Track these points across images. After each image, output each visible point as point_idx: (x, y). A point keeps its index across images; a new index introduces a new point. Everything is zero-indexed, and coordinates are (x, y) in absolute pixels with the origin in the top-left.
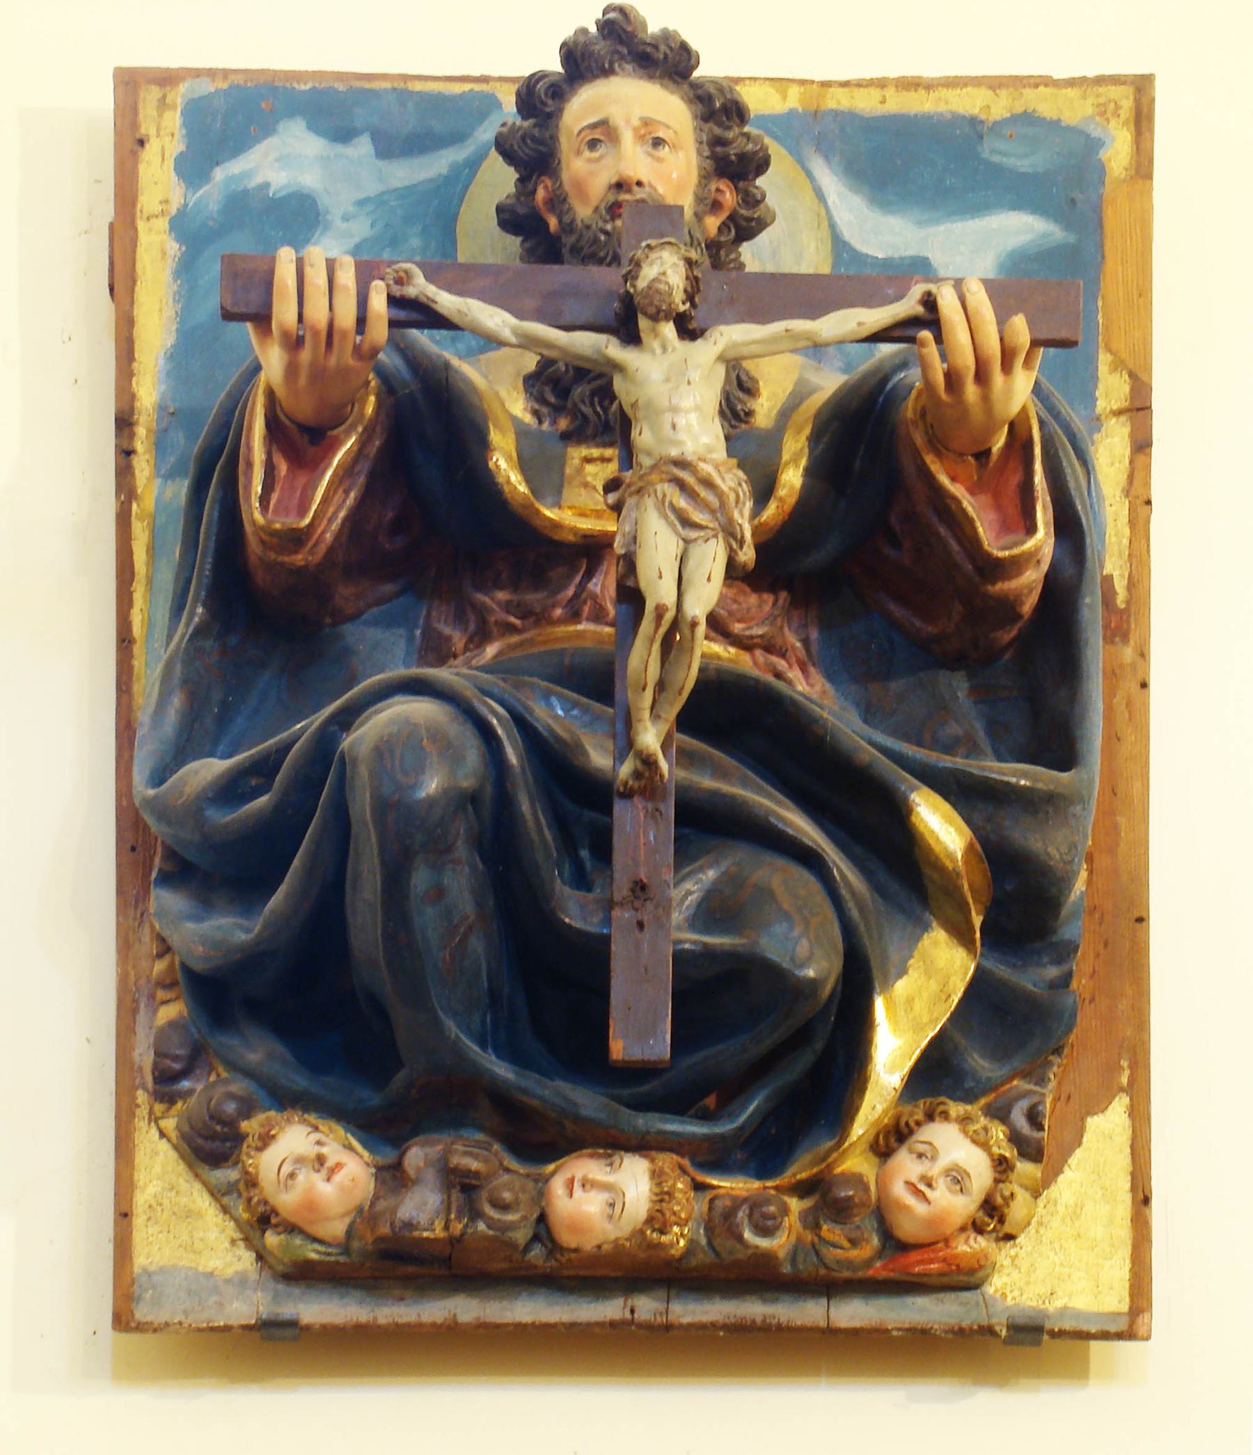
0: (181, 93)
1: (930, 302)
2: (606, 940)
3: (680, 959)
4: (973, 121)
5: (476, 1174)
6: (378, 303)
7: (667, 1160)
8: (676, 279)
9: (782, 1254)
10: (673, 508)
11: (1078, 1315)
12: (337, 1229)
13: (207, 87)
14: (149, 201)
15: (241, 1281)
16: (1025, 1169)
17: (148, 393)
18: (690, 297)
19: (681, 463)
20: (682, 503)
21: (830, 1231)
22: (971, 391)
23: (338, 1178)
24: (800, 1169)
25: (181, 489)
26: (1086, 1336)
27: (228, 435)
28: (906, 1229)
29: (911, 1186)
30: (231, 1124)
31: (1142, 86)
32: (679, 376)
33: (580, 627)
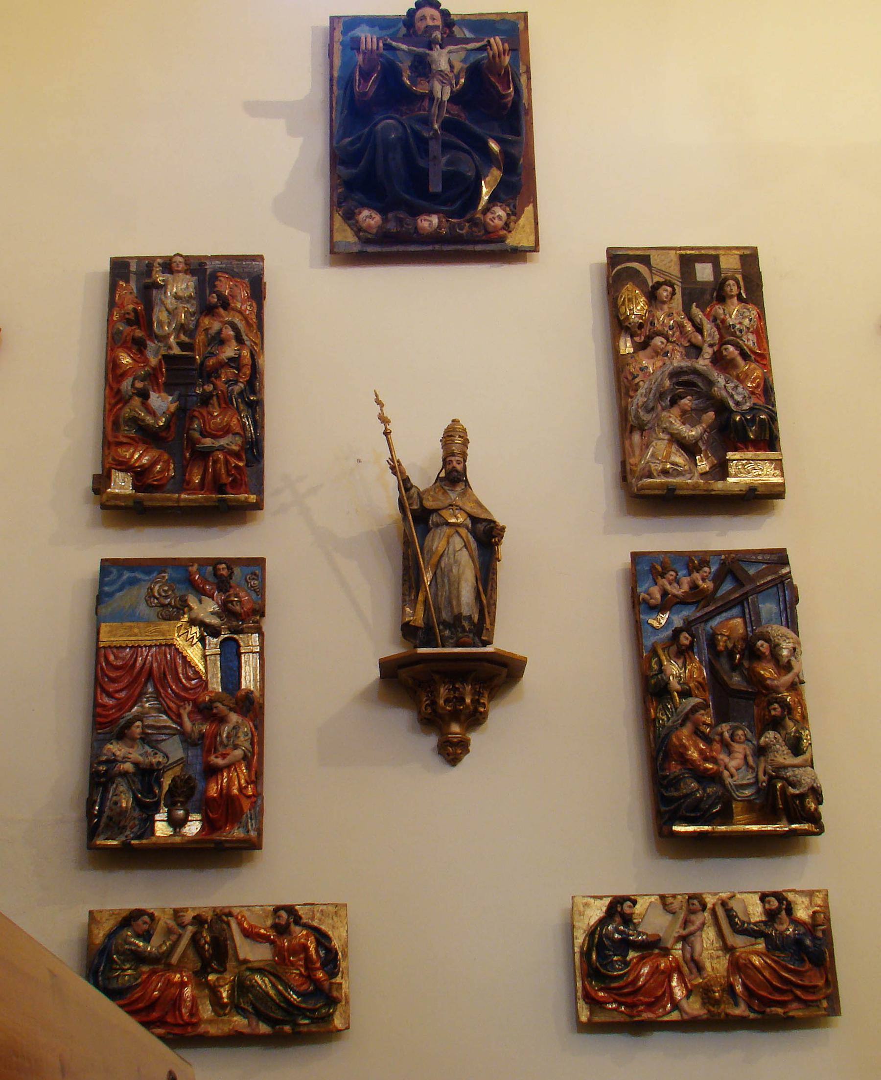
0: (342, 20)
1: (489, 42)
2: (428, 169)
3: (443, 172)
4: (493, 20)
5: (402, 218)
6: (381, 44)
7: (441, 215)
8: (439, 36)
9: (465, 234)
10: (440, 80)
11: (526, 247)
12: (374, 231)
13: (347, 19)
14: (336, 39)
15: (355, 243)
16: (513, 217)
17: (336, 74)
18: (442, 40)
19: (441, 71)
20: (441, 79)
21: (474, 229)
22: (497, 58)
23: (374, 220)
24: (468, 217)
25: (342, 92)
26: (527, 251)
27: (423, 561)
28: (490, 230)
29: (490, 219)
30: (353, 211)
31: (526, 13)
32: (440, 55)
33: (421, 112)
